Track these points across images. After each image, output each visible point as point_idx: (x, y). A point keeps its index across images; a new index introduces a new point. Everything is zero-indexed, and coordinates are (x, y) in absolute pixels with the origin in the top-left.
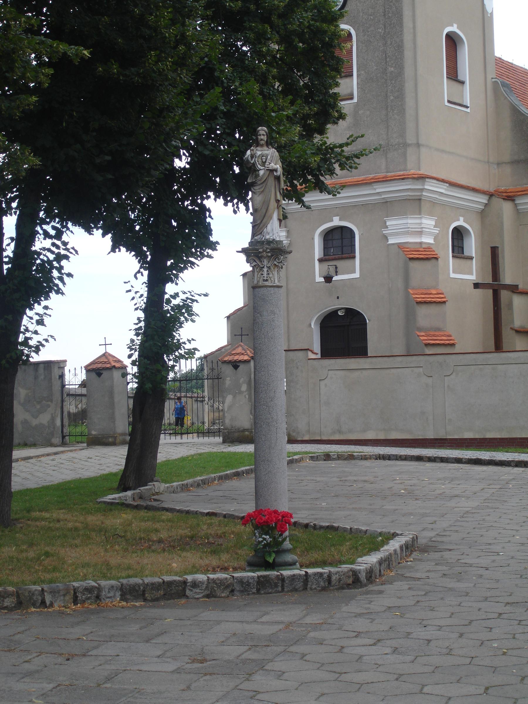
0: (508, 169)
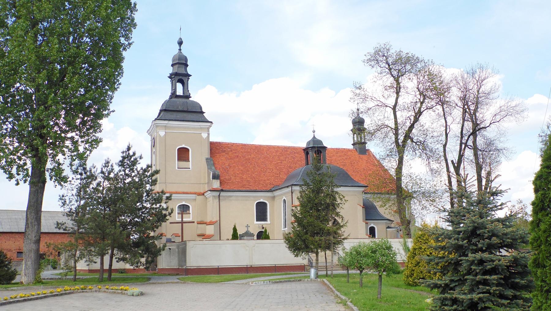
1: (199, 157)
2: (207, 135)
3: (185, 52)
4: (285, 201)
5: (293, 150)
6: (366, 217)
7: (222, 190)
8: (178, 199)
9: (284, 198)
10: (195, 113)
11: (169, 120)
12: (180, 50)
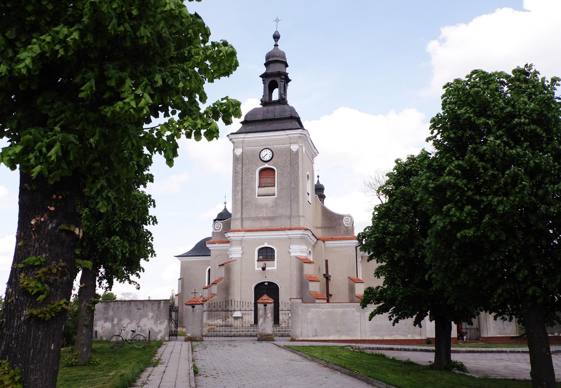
0: (320, 231)
12: (276, 45)
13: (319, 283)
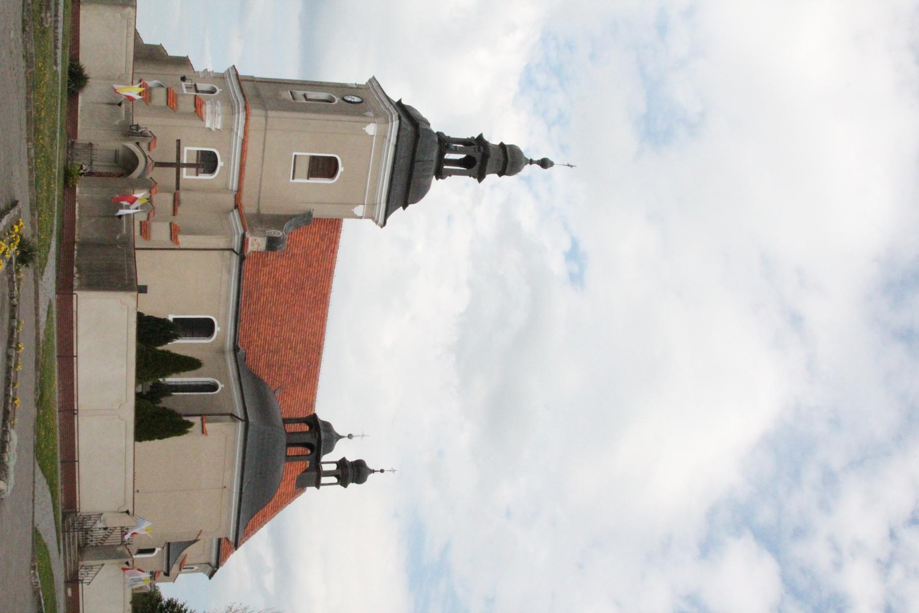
1: (313, 194)
2: (360, 214)
3: (527, 168)
4: (213, 387)
5: (312, 405)
6: (174, 544)
7: (242, 258)
8: (229, 153)
9: (218, 90)
10: (406, 188)
11: (396, 146)
12: (531, 162)
13: (165, 104)
